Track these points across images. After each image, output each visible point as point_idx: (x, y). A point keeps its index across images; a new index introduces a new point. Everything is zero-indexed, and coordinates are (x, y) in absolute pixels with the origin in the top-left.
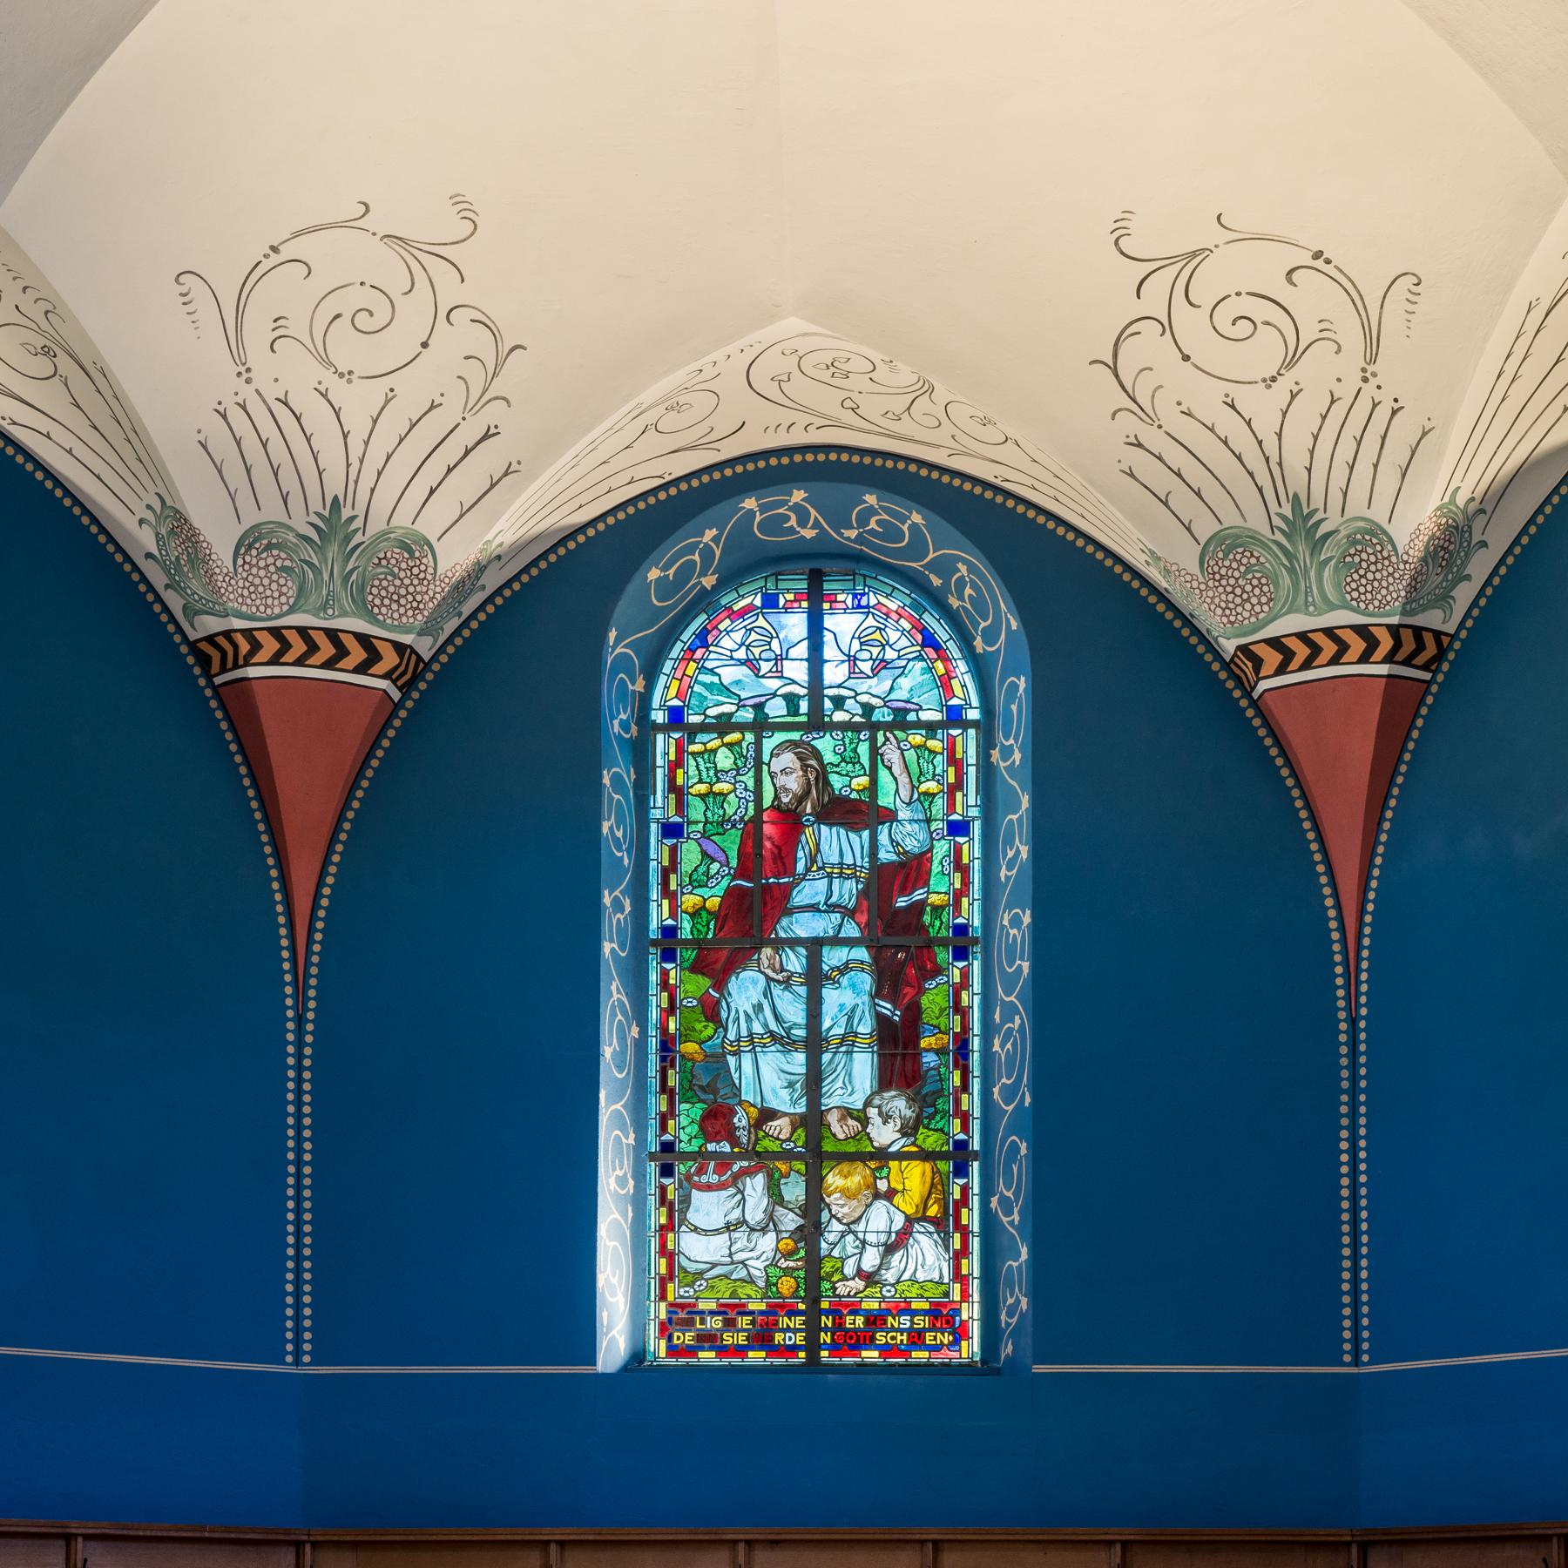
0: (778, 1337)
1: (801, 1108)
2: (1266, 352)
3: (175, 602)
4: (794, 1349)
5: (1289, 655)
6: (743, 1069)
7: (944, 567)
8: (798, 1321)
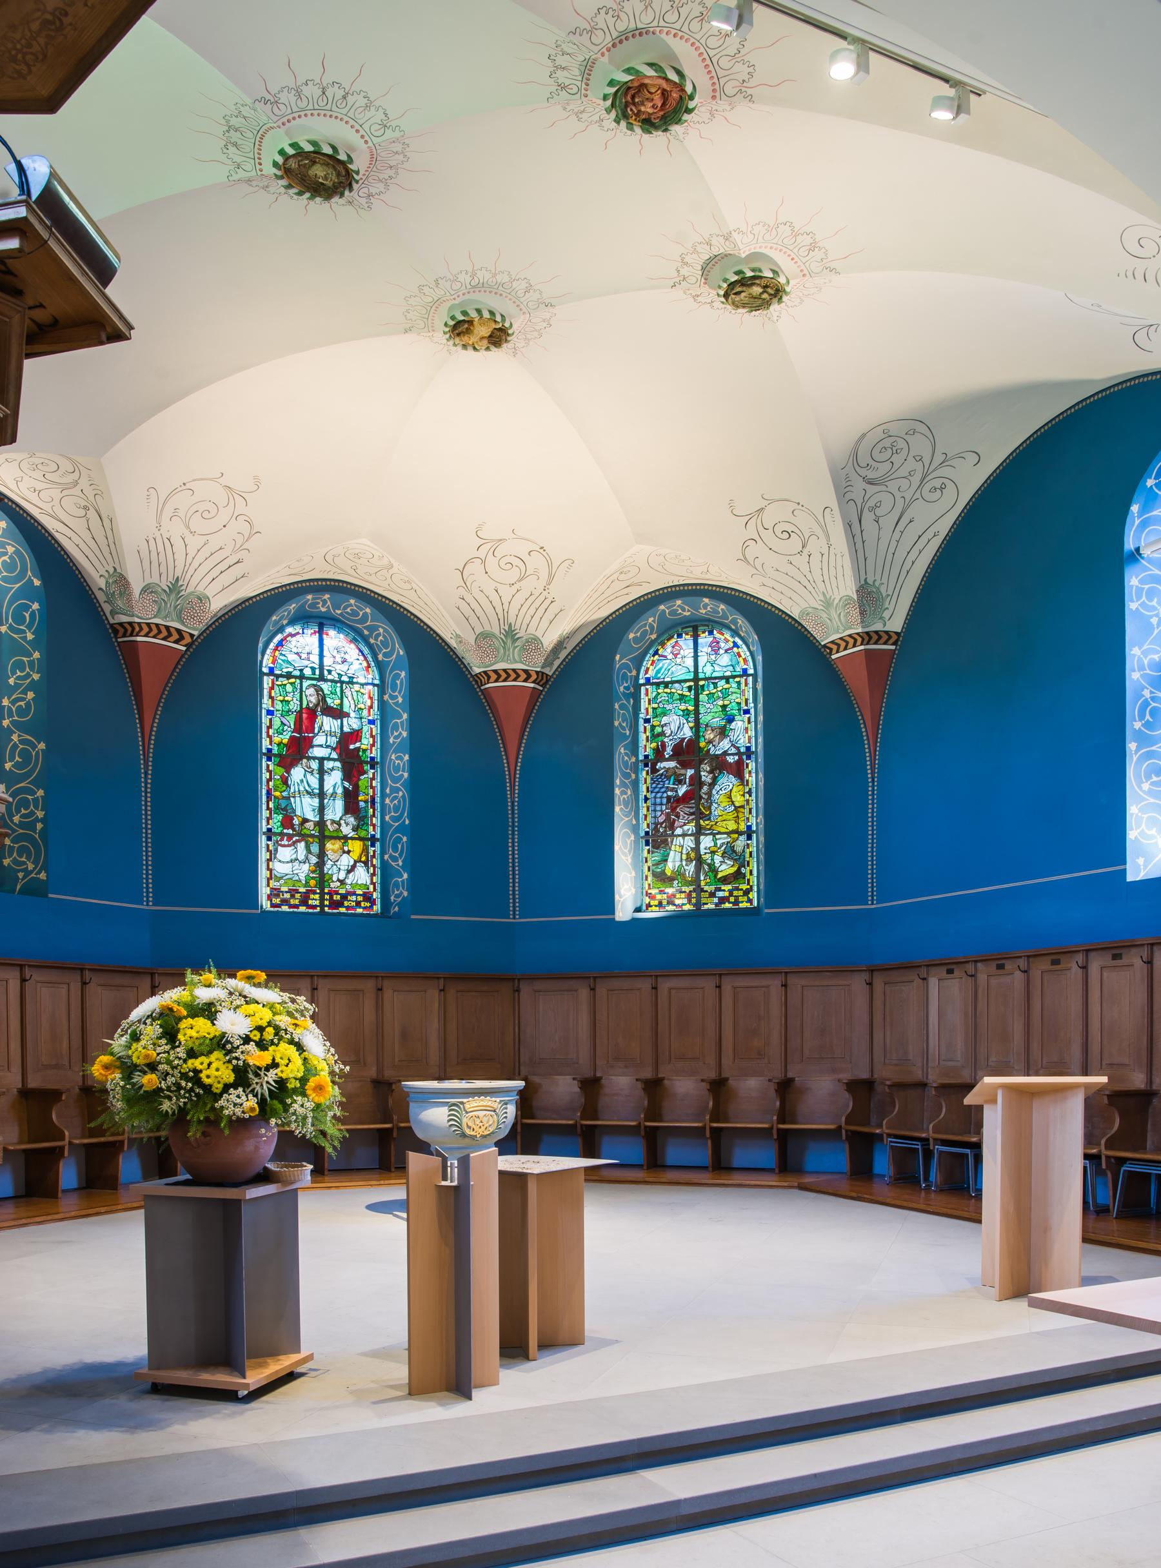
0: (310, 902)
1: (317, 819)
2: (514, 575)
3: (107, 608)
4: (314, 907)
5: (499, 676)
6: (296, 803)
7: (372, 629)
8: (317, 896)
